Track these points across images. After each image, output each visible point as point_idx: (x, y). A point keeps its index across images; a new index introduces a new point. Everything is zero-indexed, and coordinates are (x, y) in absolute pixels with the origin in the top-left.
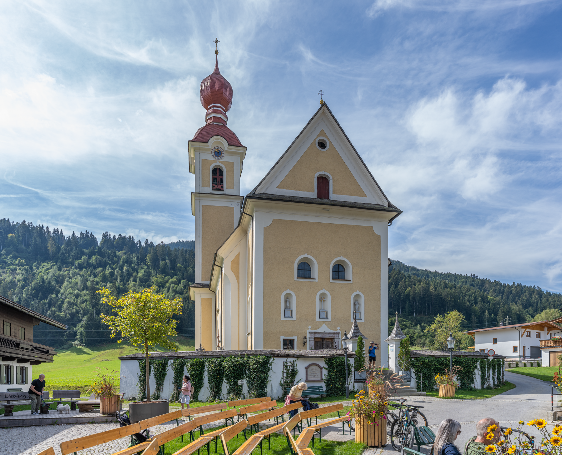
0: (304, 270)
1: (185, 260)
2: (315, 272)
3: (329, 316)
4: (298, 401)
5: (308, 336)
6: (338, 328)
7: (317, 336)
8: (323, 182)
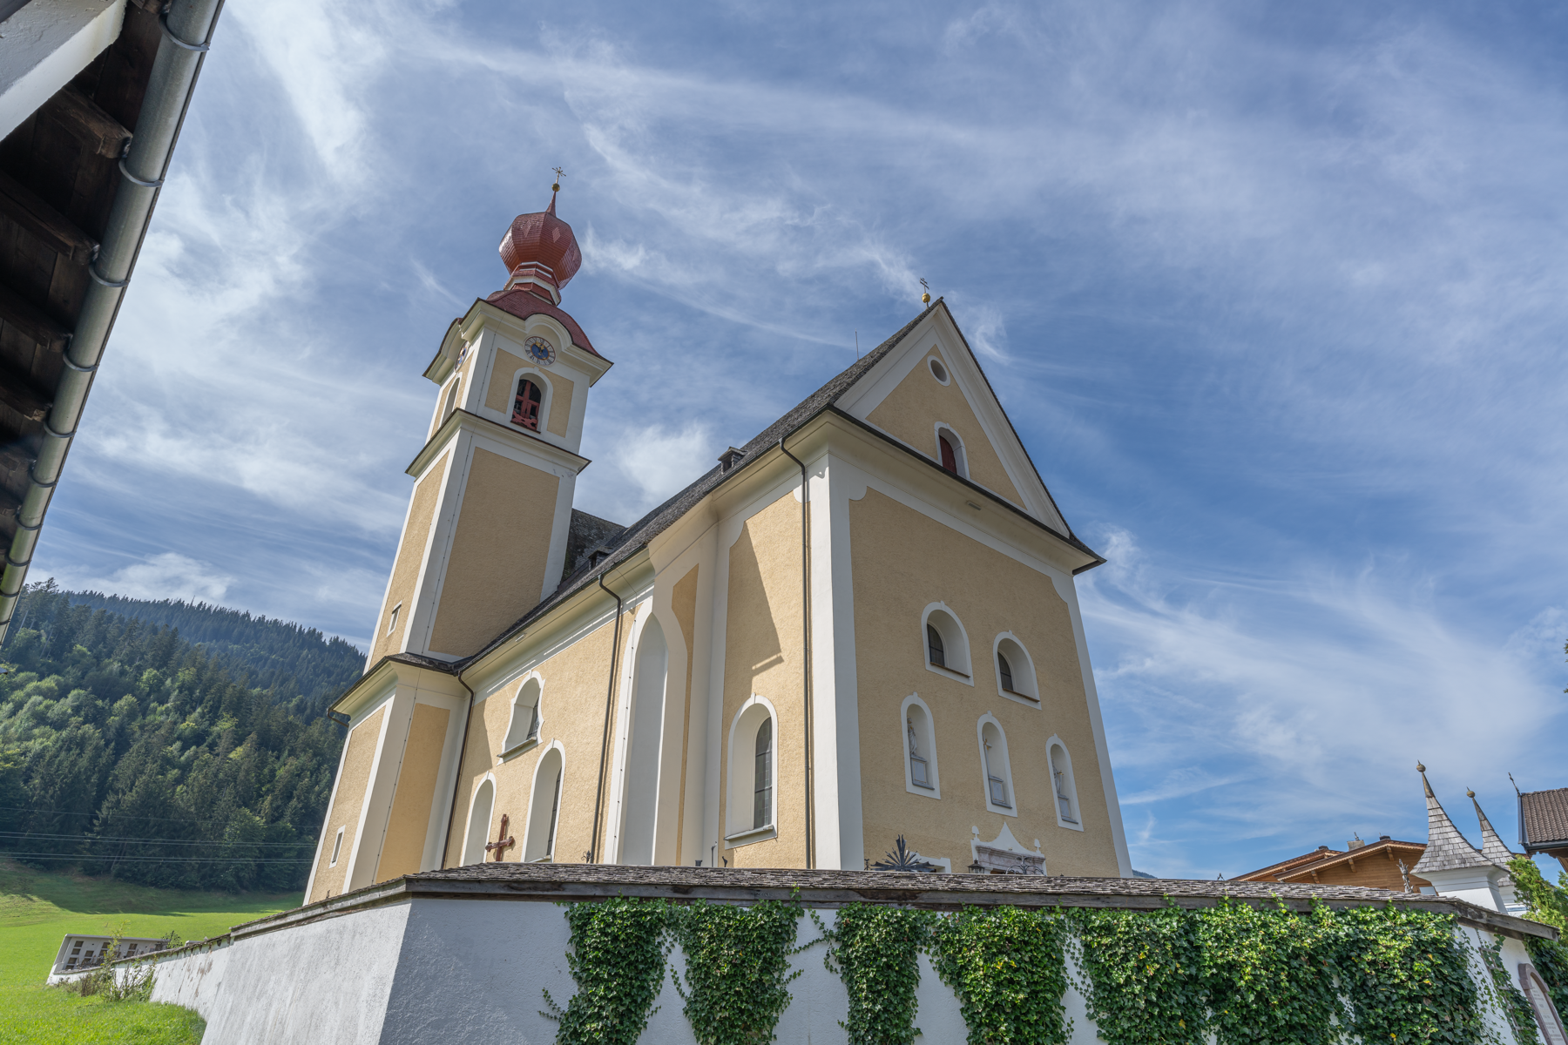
1: (101, 637)
6: (1037, 843)
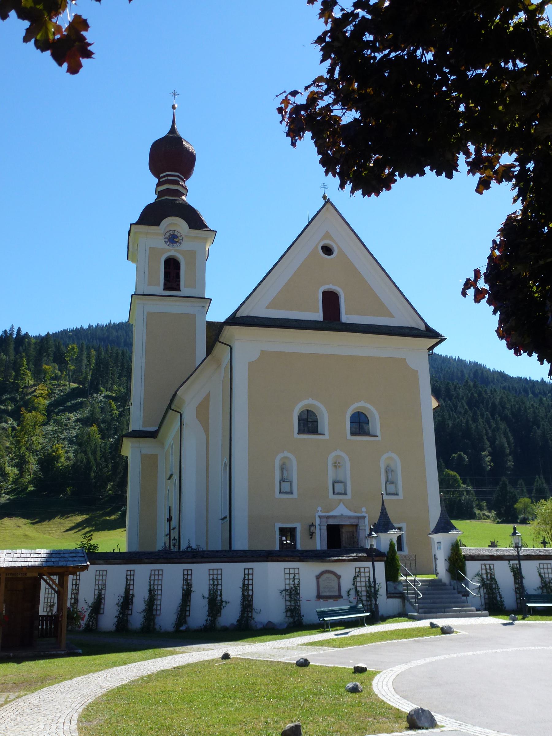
3: (349, 491)
4: (341, 482)
5: (317, 522)
7: (332, 522)
8: (331, 300)
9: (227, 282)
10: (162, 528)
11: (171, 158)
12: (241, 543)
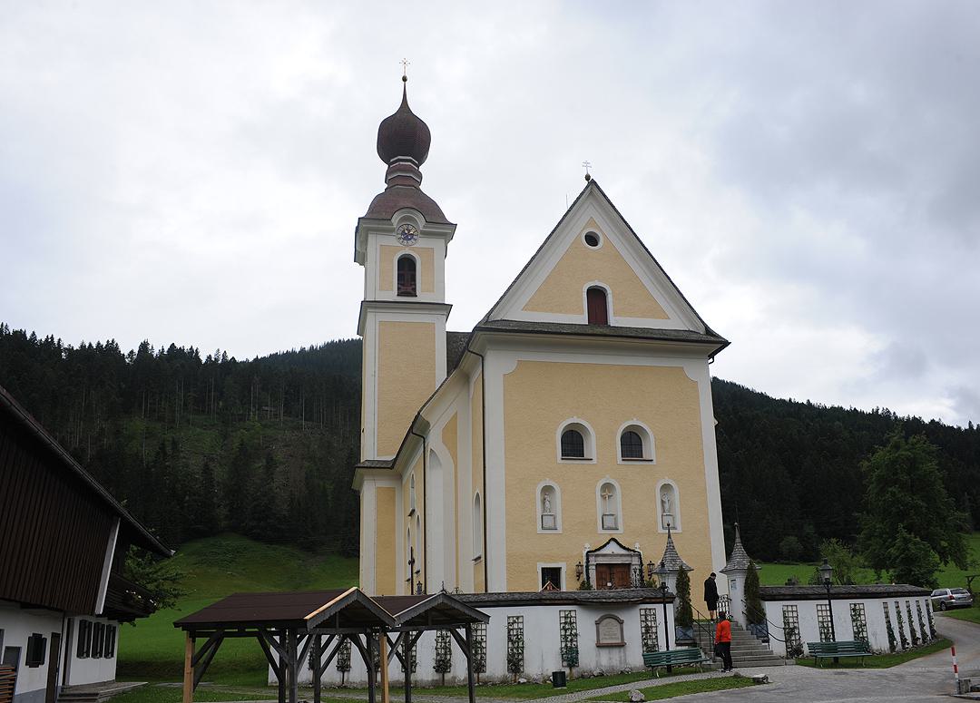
0: (573, 444)
2: (591, 447)
3: (620, 527)
8: (597, 297)
9: (472, 284)
10: (403, 572)
11: (403, 139)
12: (498, 586)
